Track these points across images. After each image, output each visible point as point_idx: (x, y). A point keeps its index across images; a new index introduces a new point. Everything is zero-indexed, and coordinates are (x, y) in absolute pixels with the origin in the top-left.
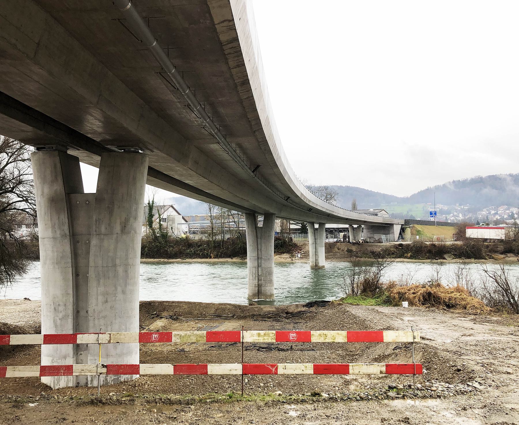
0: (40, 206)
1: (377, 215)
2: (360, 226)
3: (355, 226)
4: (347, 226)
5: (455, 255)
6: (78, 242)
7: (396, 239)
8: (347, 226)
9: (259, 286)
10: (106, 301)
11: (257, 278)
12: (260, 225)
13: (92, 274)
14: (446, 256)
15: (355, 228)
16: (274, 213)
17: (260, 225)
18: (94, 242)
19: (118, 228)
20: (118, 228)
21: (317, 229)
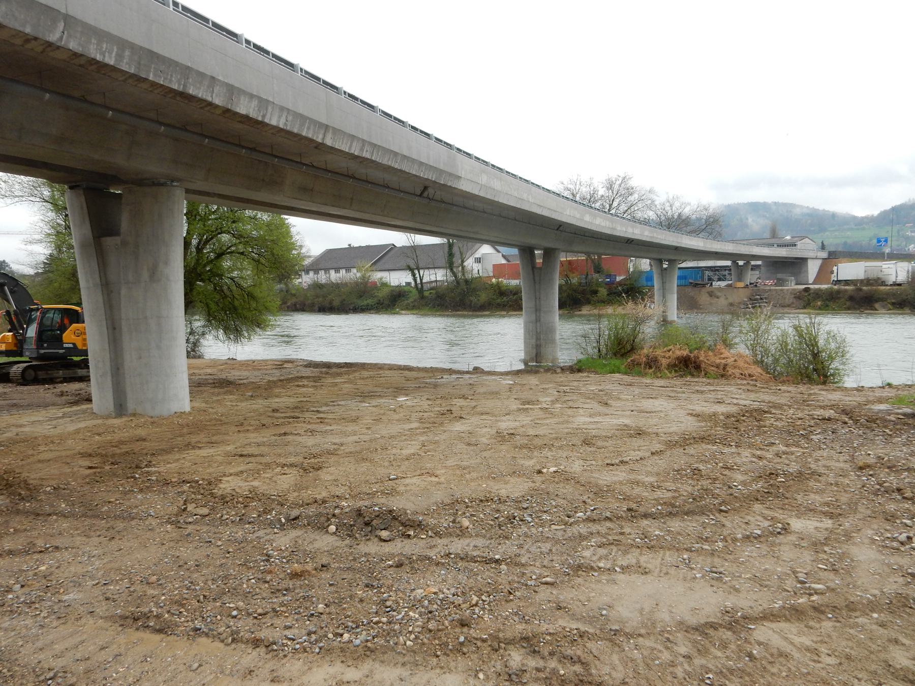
0: (75, 240)
1: (795, 245)
2: (748, 262)
3: (741, 263)
4: (728, 263)
5: (893, 304)
6: (112, 292)
7: (811, 280)
8: (728, 263)
9: (538, 347)
10: (140, 358)
11: (534, 337)
12: (539, 261)
13: (125, 328)
14: (877, 305)
15: (741, 266)
16: (554, 247)
17: (539, 261)
18: (123, 292)
19: (145, 275)
20: (145, 275)
21: (666, 269)
